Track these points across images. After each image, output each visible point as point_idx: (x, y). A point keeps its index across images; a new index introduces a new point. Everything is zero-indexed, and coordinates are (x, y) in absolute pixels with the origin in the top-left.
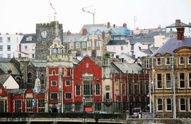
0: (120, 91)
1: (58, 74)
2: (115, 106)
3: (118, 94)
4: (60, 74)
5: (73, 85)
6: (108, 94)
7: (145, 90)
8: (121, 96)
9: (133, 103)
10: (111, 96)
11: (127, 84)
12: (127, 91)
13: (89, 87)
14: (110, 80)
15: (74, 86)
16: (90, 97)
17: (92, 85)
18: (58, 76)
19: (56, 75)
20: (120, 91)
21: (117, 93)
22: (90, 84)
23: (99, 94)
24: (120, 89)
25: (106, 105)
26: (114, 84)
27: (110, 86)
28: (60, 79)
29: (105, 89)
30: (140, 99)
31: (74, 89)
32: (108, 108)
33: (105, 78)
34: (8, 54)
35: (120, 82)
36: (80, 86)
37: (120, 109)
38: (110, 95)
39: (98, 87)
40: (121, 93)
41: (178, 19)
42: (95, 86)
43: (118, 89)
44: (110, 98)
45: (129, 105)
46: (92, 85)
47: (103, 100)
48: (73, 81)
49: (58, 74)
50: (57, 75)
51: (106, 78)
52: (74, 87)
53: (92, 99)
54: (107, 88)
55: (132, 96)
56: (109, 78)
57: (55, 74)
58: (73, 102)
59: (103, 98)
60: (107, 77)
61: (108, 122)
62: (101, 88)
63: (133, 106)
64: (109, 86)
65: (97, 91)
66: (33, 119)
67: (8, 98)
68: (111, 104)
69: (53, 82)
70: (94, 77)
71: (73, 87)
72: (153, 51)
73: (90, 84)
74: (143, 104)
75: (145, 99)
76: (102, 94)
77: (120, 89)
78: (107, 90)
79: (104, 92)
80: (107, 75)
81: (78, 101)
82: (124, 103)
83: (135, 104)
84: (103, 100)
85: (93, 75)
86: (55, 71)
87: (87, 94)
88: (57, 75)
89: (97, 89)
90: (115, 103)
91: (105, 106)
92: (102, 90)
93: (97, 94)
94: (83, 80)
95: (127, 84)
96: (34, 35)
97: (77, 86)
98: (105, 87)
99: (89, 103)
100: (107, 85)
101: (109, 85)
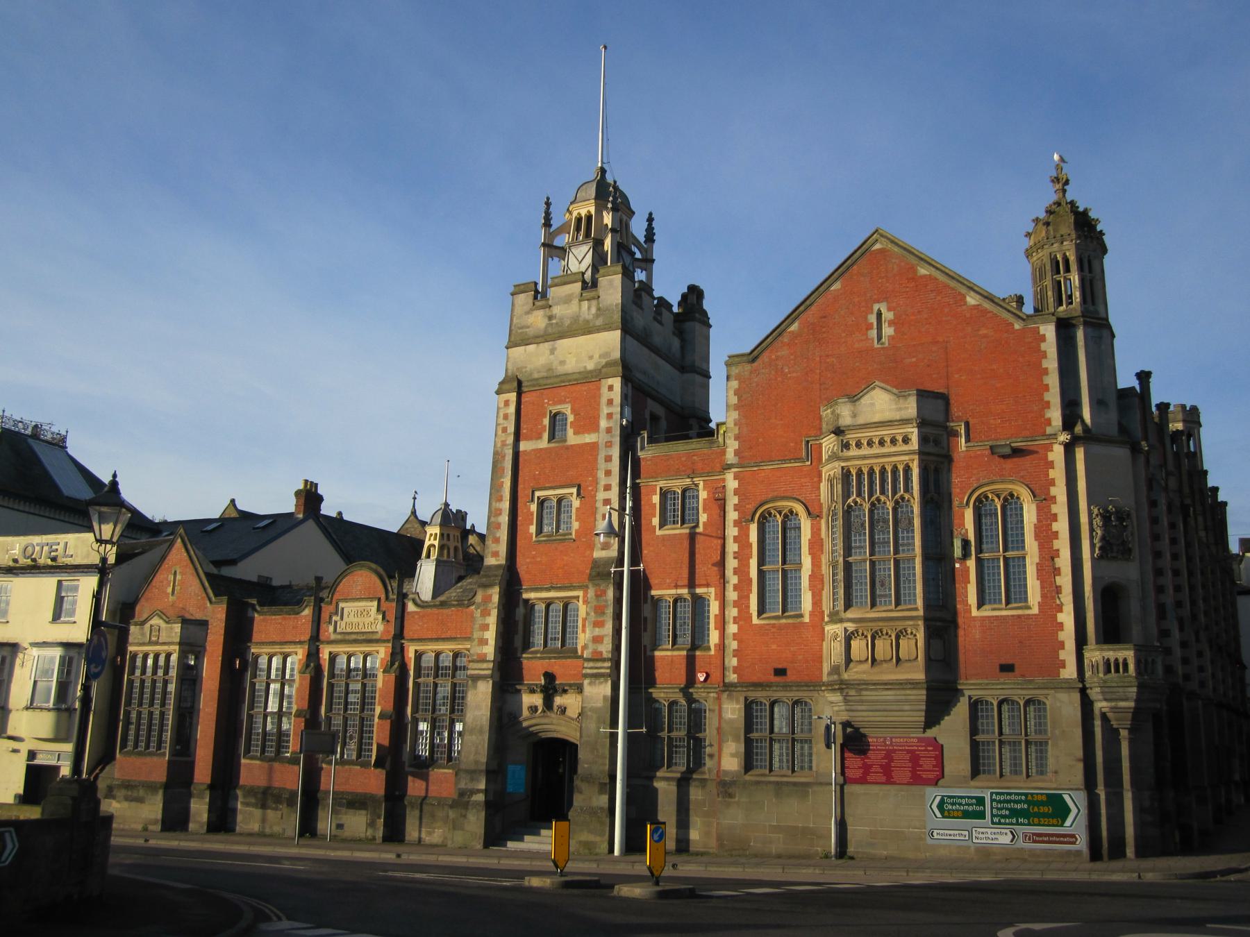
1: (594, 427)
4: (609, 430)
5: (732, 515)
13: (871, 483)
15: (741, 524)
18: (594, 447)
19: (573, 439)
28: (608, 473)
34: (49, 615)
36: (806, 525)
41: (319, 575)
48: (732, 484)
49: (594, 427)
50: (589, 438)
52: (742, 539)
57: (570, 431)
58: (732, 677)
61: (1116, 877)
67: (98, 803)
69: (664, 494)
71: (731, 532)
72: (1039, 787)
81: (780, 672)
86: (567, 409)
88: (589, 438)
96: (47, 457)
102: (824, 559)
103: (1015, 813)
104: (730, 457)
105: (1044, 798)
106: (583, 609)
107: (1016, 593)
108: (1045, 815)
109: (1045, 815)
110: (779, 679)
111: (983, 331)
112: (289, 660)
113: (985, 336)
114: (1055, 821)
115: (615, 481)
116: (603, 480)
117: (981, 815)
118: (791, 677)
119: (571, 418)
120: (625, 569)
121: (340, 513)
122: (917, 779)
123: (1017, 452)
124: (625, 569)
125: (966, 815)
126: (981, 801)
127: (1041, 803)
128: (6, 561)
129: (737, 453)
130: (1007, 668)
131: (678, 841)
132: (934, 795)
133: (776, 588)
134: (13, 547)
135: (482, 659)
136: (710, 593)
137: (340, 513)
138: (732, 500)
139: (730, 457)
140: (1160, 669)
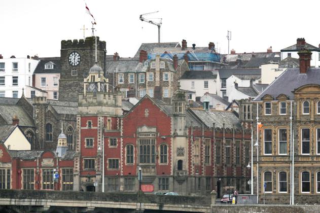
0: (202, 157)
2: (192, 182)
3: (197, 163)
5: (122, 146)
9: (222, 178)
10: (185, 166)
11: (213, 146)
12: (212, 158)
13: (149, 150)
15: (124, 147)
17: (153, 147)
19: (92, 128)
22: (151, 145)
24: (202, 154)
25: (177, 180)
27: (185, 149)
29: (176, 155)
33: (176, 136)
34: (14, 90)
35: (201, 142)
37: (201, 187)
38: (184, 164)
39: (164, 149)
42: (159, 149)
43: (197, 154)
44: (184, 169)
45: (216, 181)
46: (153, 147)
47: (172, 172)
48: (122, 140)
49: (97, 126)
52: (124, 150)
53: (153, 170)
54: (180, 152)
55: (222, 167)
56: (182, 135)
57: (92, 126)
59: (172, 169)
60: (179, 133)
62: (170, 152)
65: (162, 156)
67: (12, 166)
70: (157, 133)
71: (122, 149)
76: (170, 161)
77: (202, 154)
79: (175, 158)
80: (180, 130)
81: (130, 174)
82: (207, 179)
83: (225, 179)
84: (172, 172)
85: (155, 129)
86: (91, 121)
91: (176, 183)
92: (170, 155)
93: (162, 162)
95: (213, 146)
97: (128, 147)
98: (176, 150)
100: (179, 147)
102: (137, 154)
104: (122, 135)
106: (95, 162)
107: (166, 161)
115: (101, 137)
116: (98, 137)
119: (92, 123)
120: (103, 155)
123: (87, 8)
124: (103, 155)
129: (123, 134)
130: (163, 173)
133: (130, 159)
134: (1, 199)
135: (76, 171)
136: (94, 72)
138: (122, 143)
139: (122, 135)
140: (182, 105)
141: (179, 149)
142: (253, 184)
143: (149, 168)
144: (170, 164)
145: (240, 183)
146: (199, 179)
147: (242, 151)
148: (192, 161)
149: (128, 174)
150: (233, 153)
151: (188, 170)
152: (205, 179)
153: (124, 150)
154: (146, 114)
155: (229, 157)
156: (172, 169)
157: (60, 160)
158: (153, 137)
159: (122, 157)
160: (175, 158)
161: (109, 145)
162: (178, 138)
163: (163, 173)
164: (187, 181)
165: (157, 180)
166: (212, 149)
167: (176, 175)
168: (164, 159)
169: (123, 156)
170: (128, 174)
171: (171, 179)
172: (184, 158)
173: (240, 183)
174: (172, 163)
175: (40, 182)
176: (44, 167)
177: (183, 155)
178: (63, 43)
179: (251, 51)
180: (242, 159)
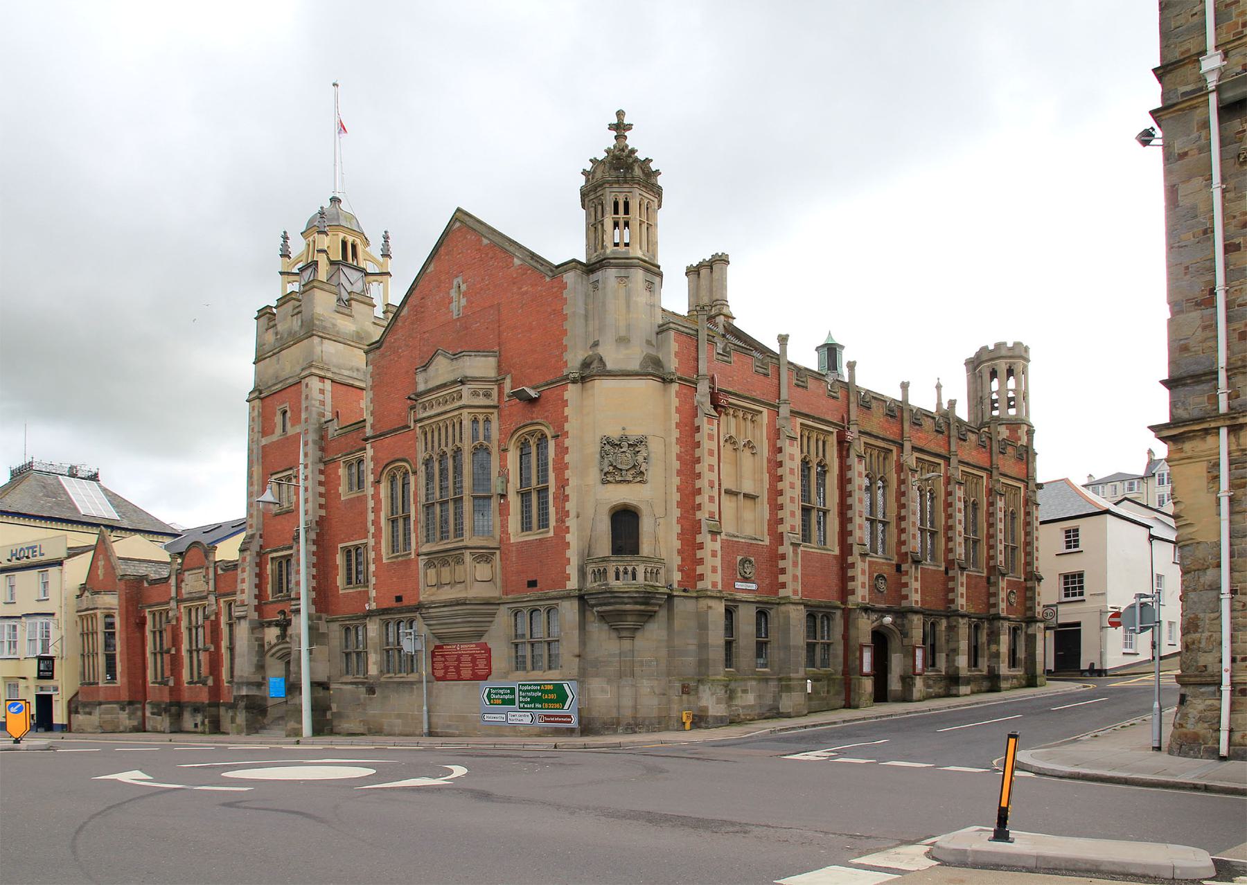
0: (776, 507)
2: (703, 627)
3: (749, 530)
6: (625, 522)
7: (1001, 536)
8: (786, 549)
9: (902, 614)
10: (660, 536)
11: (844, 468)
12: (845, 520)
14: (648, 386)
16: (468, 557)
17: (481, 450)
20: (776, 507)
21: (738, 518)
22: (467, 446)
23: (544, 523)
24: (775, 493)
25: (603, 617)
26: (849, 468)
27: (655, 447)
29: (594, 475)
30: (962, 590)
31: (376, 510)
32: (627, 644)
33: (591, 371)
35: (776, 434)
37: (774, 652)
38: (646, 525)
39: (533, 445)
40: (792, 519)
42: (513, 457)
43: (748, 487)
44: (646, 548)
45: (865, 626)
46: (481, 450)
47: (572, 570)
51: (610, 366)
53: (483, 571)
54: (622, 459)
55: (898, 567)
56: (635, 366)
59: (573, 555)
60: (613, 357)
62: (561, 467)
63: (905, 634)
64: (637, 445)
65: (525, 496)
66: (256, 413)
68: (649, 606)
70: (499, 382)
73: (467, 446)
74: (977, 627)
75: (995, 595)
76: (563, 515)
77: (775, 493)
78: (612, 474)
79: (589, 500)
80: (623, 341)
81: (399, 599)
82: (811, 616)
83: (917, 620)
84: (572, 570)
85: (492, 361)
87: (444, 536)
89: (524, 479)
90: (703, 603)
91: (598, 631)
92: (563, 483)
93: (526, 526)
94: (400, 611)
95: (844, 468)
97: (393, 480)
98: (594, 449)
99: (458, 603)
100: (614, 433)
101: (634, 432)
103: (534, 700)
105: (551, 687)
108: (551, 701)
109: (551, 701)
110: (399, 604)
111: (524, 289)
112: (984, 474)
113: (526, 293)
114: (557, 706)
117: (512, 702)
118: (405, 602)
121: (996, 365)
122: (476, 677)
125: (505, 702)
126: (512, 691)
127: (550, 692)
128: (1, 559)
130: (532, 584)
131: (814, 651)
132: (485, 686)
137: (996, 365)
141: (610, 444)
142: (300, 722)
143: (459, 561)
144: (562, 529)
145: (983, 638)
146: (762, 614)
147: (991, 515)
148: (702, 515)
149: (394, 604)
150: (949, 516)
151: (677, 560)
152: (797, 616)
153: (376, 497)
154: (568, 356)
155: (975, 542)
156: (573, 555)
157: (220, 572)
158: (482, 401)
159: (372, 530)
160: (589, 500)
161: (341, 490)
162: (602, 386)
163: (532, 584)
164: (670, 618)
165: (503, 617)
166: (844, 481)
167: (591, 585)
168: (537, 499)
169: (376, 523)
170: (394, 604)
171: (569, 611)
172: (654, 496)
173: (983, 638)
174: (571, 522)
175: (178, 650)
176: (192, 600)
177: (639, 475)
178: (458, 210)
179: (1037, 446)
180: (991, 547)
